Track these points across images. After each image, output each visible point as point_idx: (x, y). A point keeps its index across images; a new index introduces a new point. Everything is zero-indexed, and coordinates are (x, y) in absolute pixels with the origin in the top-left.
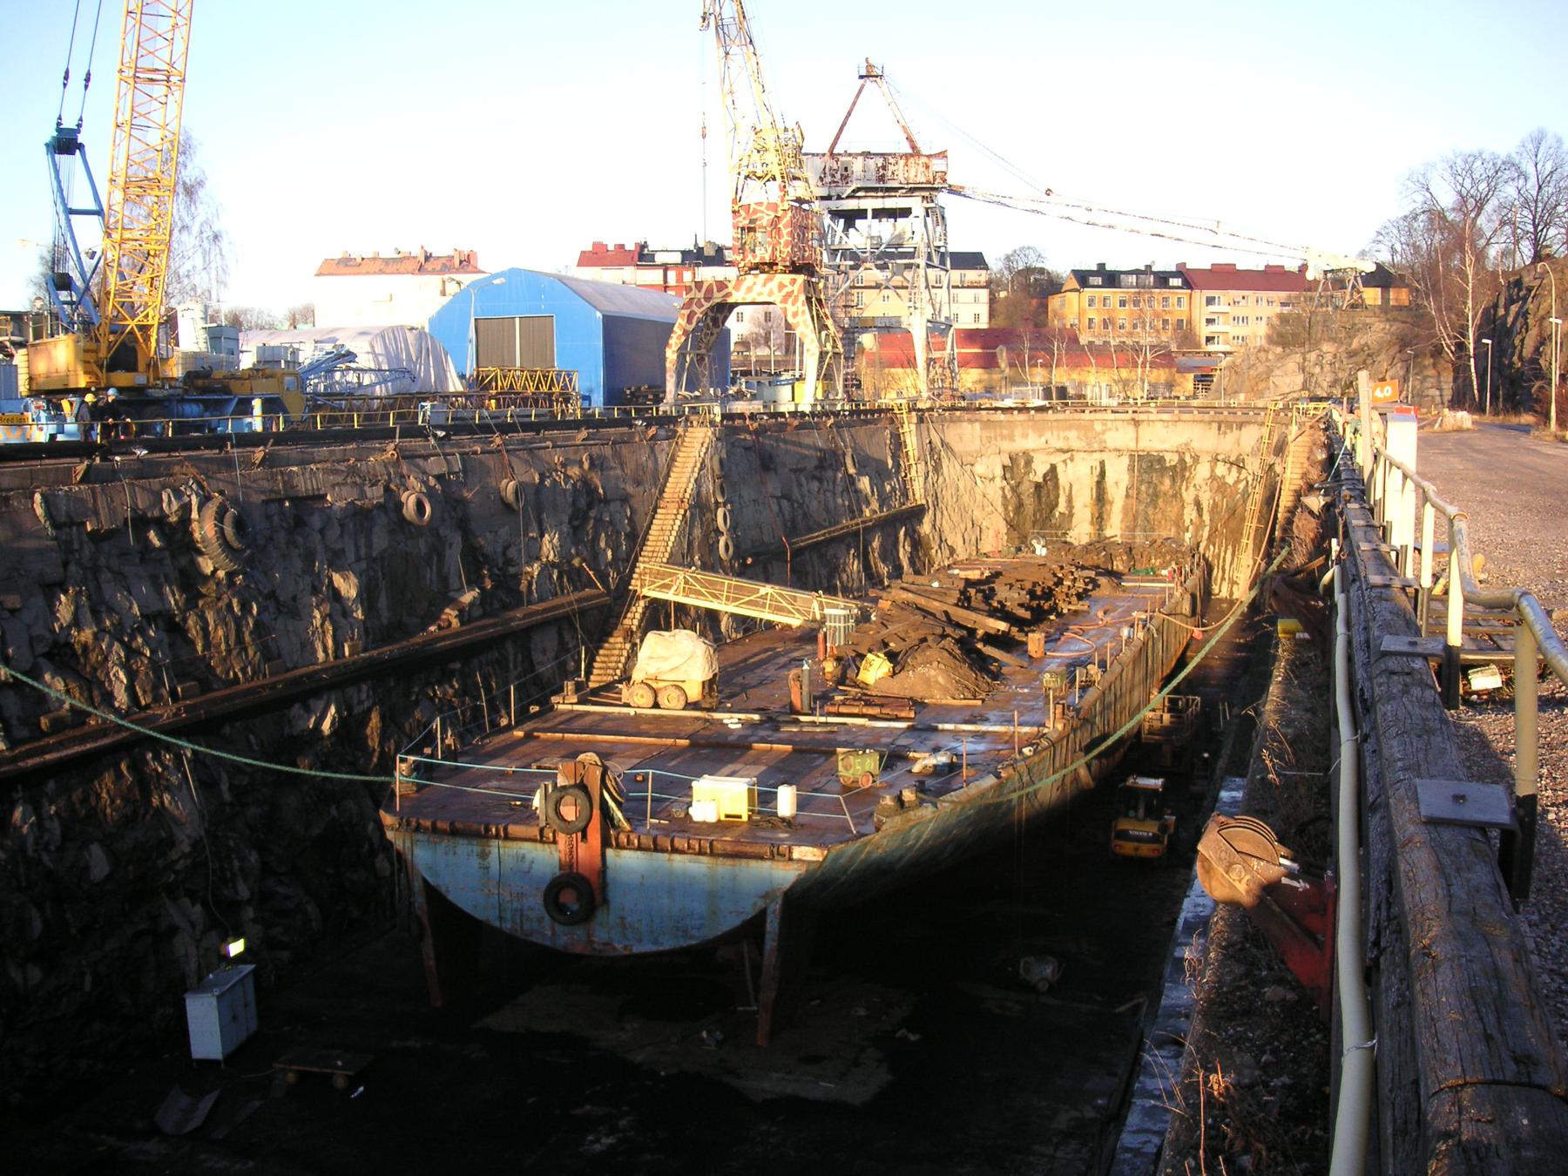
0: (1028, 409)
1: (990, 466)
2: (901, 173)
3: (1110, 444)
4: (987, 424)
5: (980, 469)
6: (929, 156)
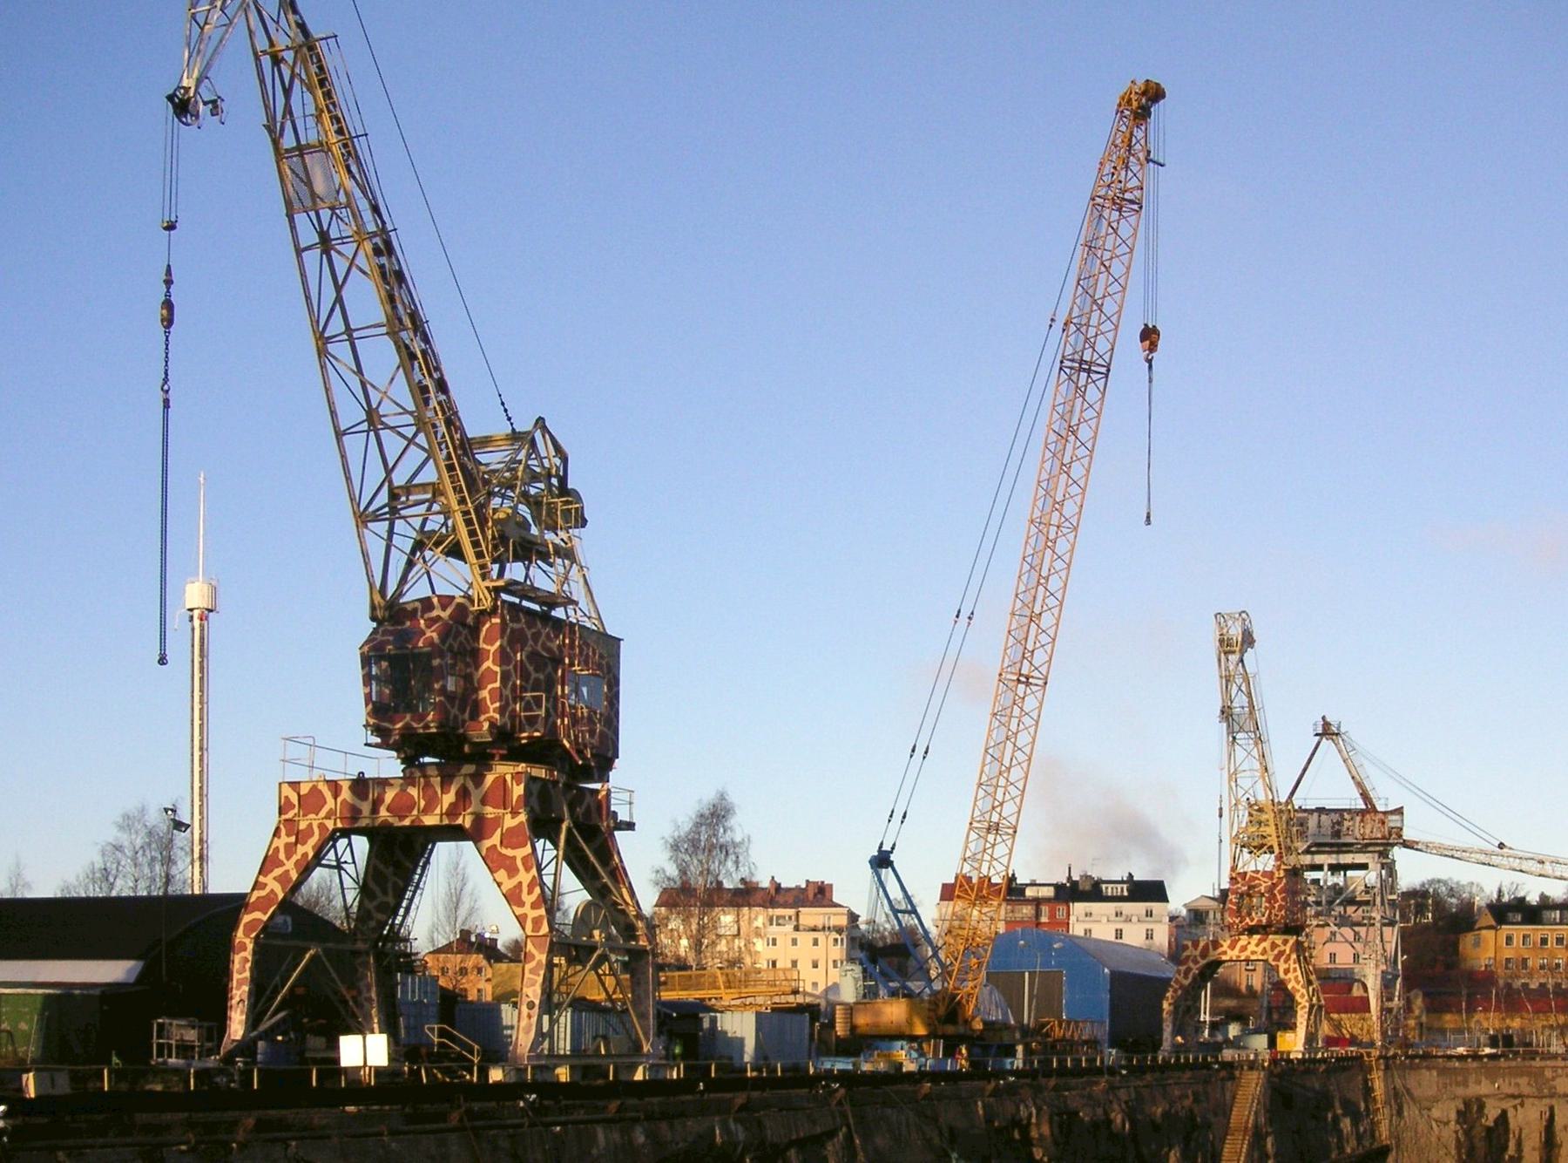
0: (1482, 1057)
1: (1447, 1110)
2: (1357, 830)
3: (1561, 1090)
4: (1443, 1072)
5: (1436, 1113)
6: (1385, 813)
